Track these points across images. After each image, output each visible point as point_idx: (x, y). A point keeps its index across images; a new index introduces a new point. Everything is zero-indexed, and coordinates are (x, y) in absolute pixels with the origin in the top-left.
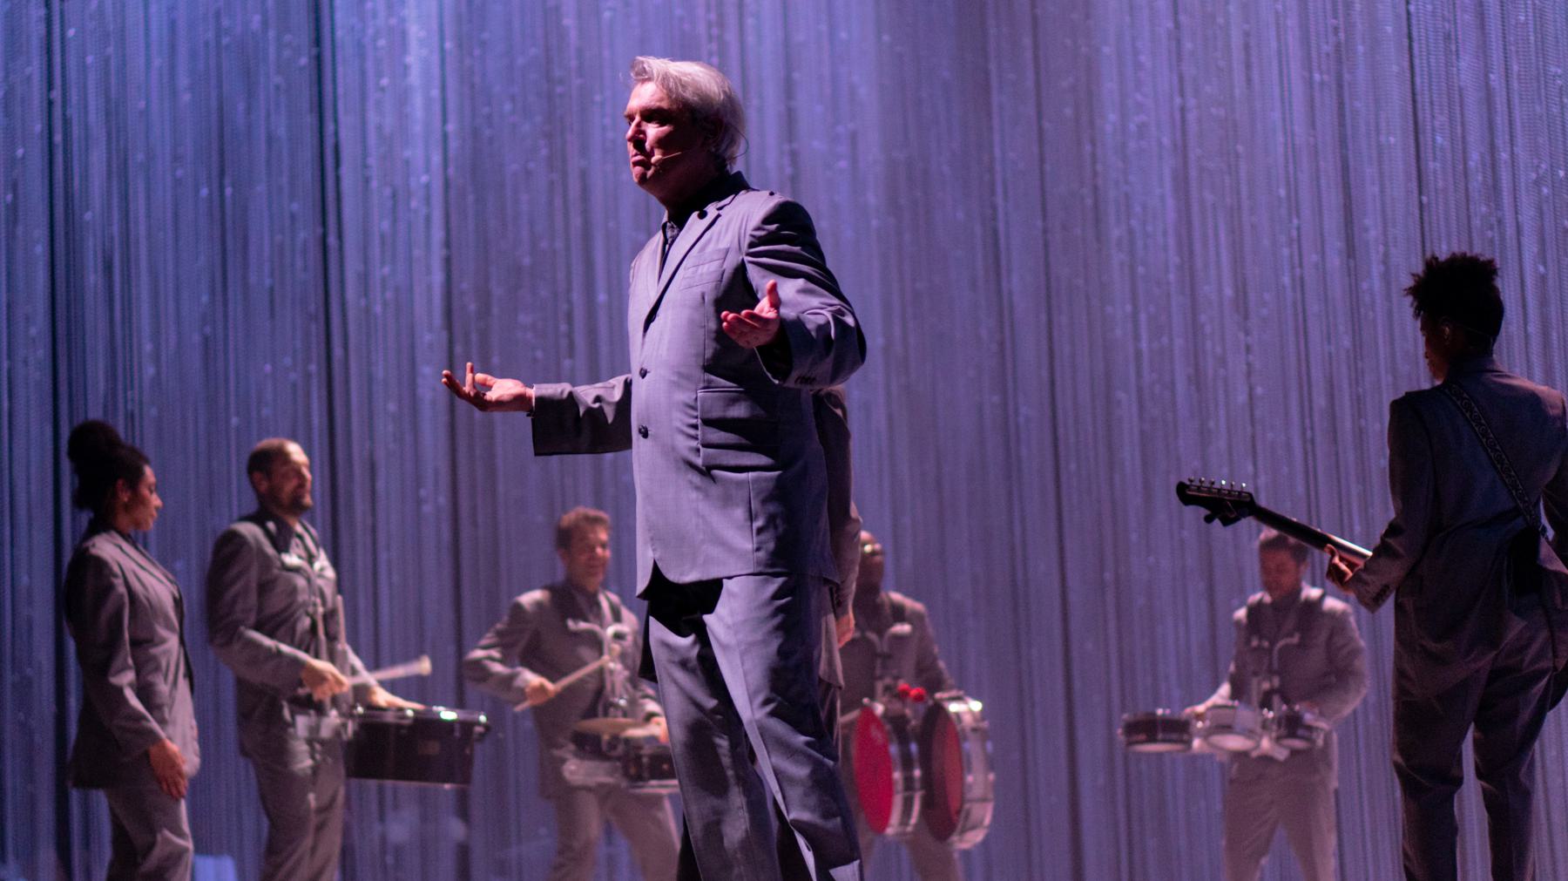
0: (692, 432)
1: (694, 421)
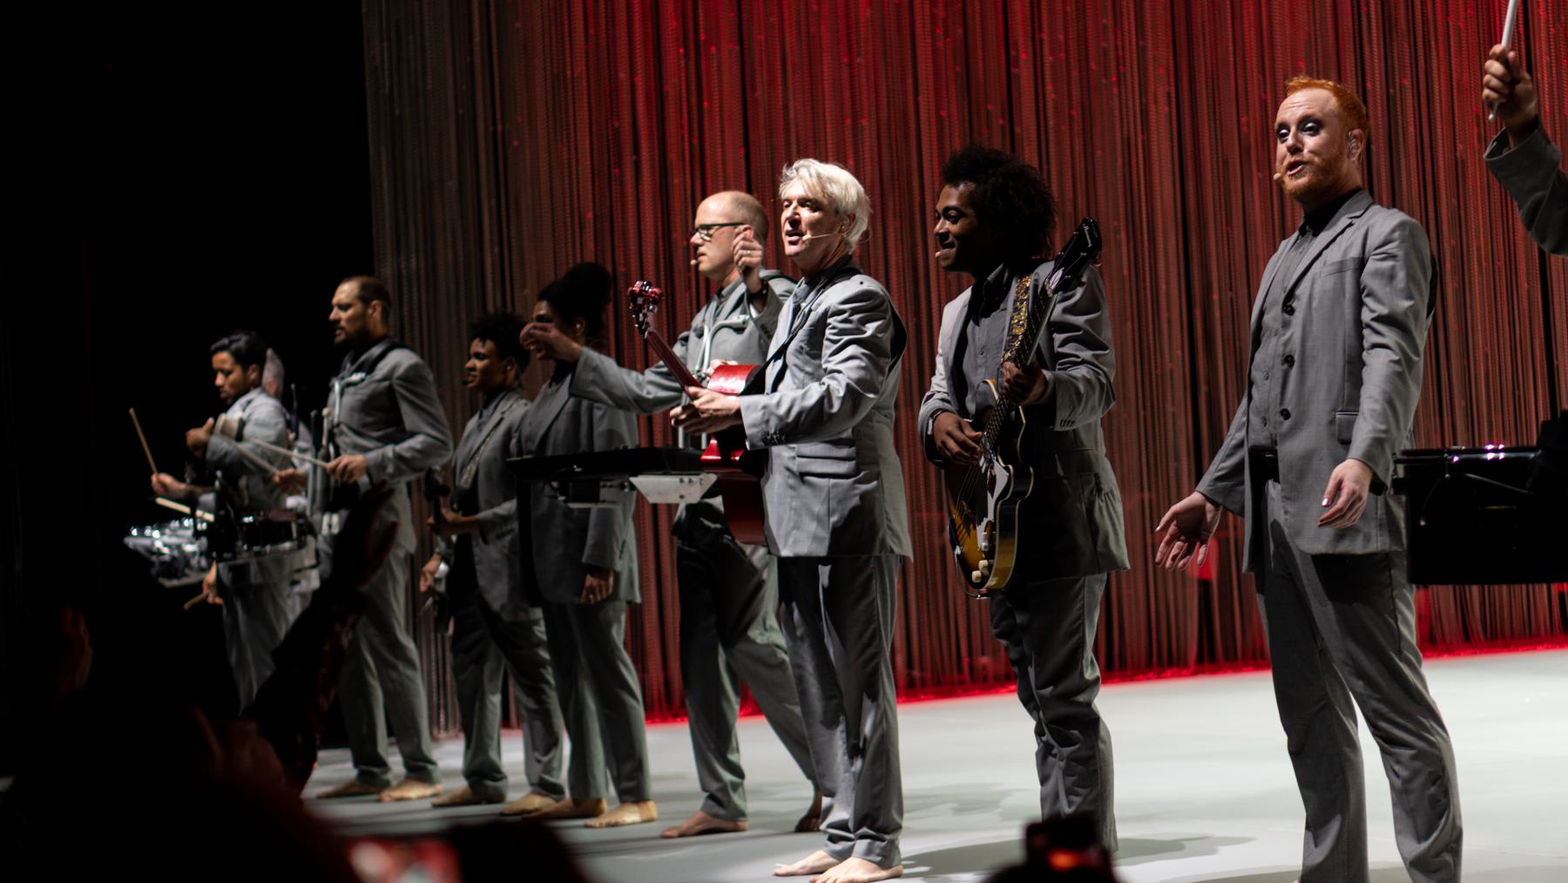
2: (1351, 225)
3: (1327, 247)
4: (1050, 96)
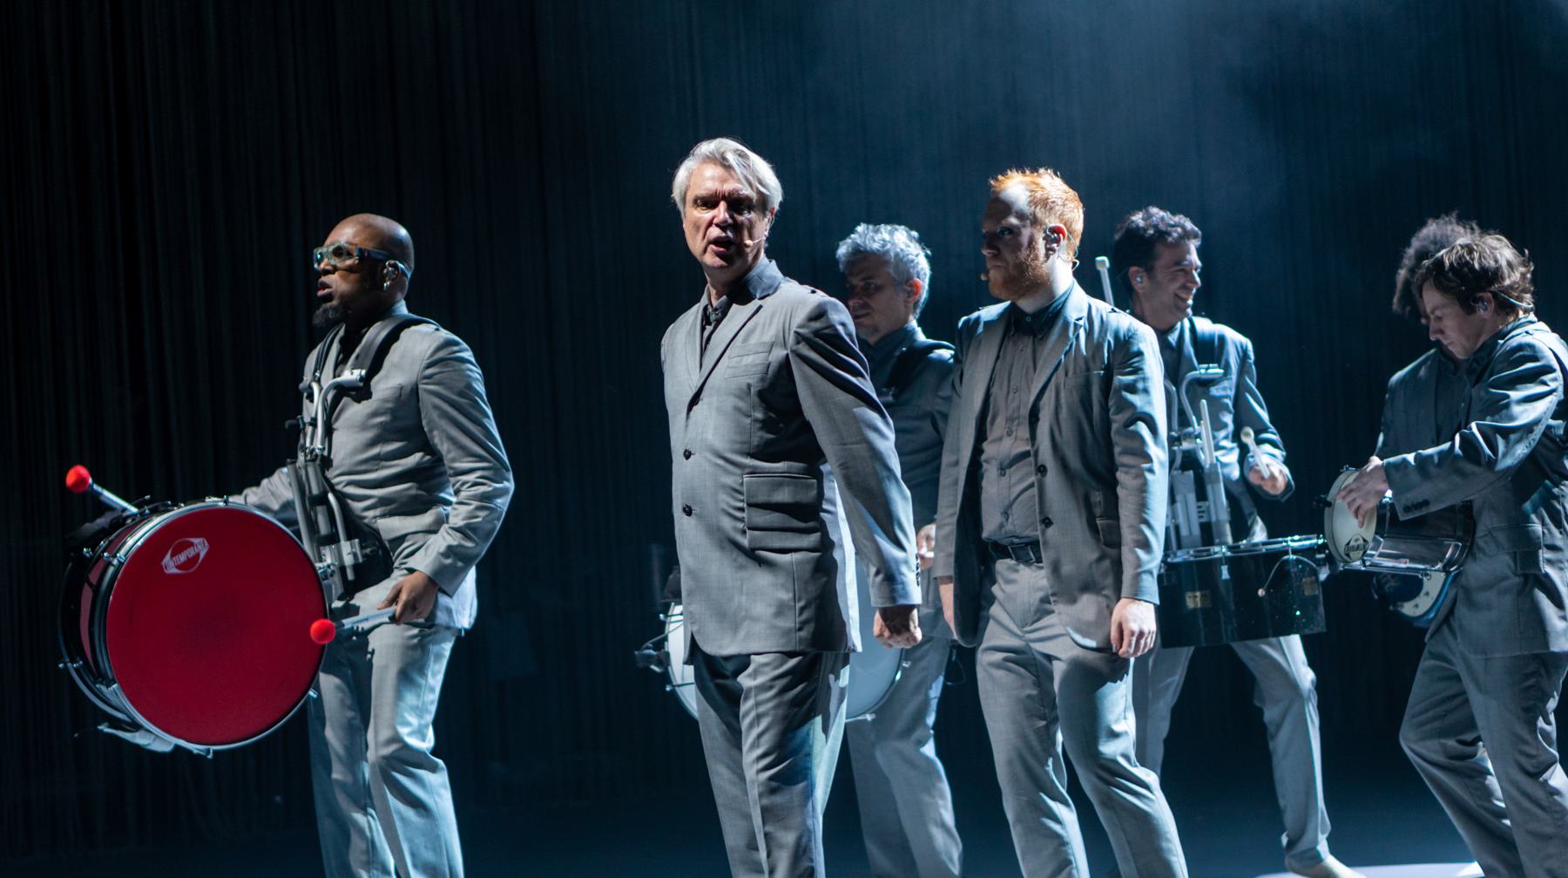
0: (739, 514)
1: (740, 505)
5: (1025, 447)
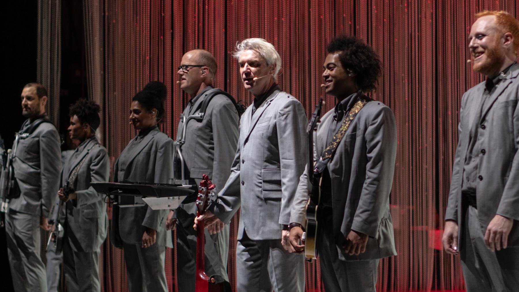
0: (260, 185)
1: (260, 181)
2: (511, 82)
3: (500, 94)
4: (374, 12)
5: (119, 180)
